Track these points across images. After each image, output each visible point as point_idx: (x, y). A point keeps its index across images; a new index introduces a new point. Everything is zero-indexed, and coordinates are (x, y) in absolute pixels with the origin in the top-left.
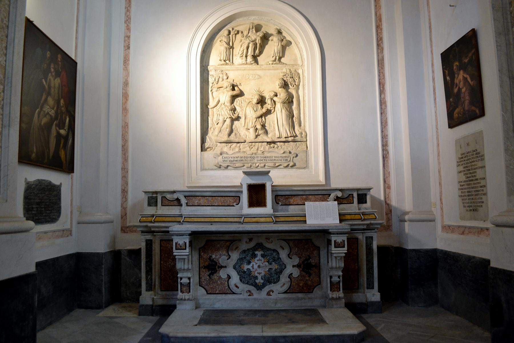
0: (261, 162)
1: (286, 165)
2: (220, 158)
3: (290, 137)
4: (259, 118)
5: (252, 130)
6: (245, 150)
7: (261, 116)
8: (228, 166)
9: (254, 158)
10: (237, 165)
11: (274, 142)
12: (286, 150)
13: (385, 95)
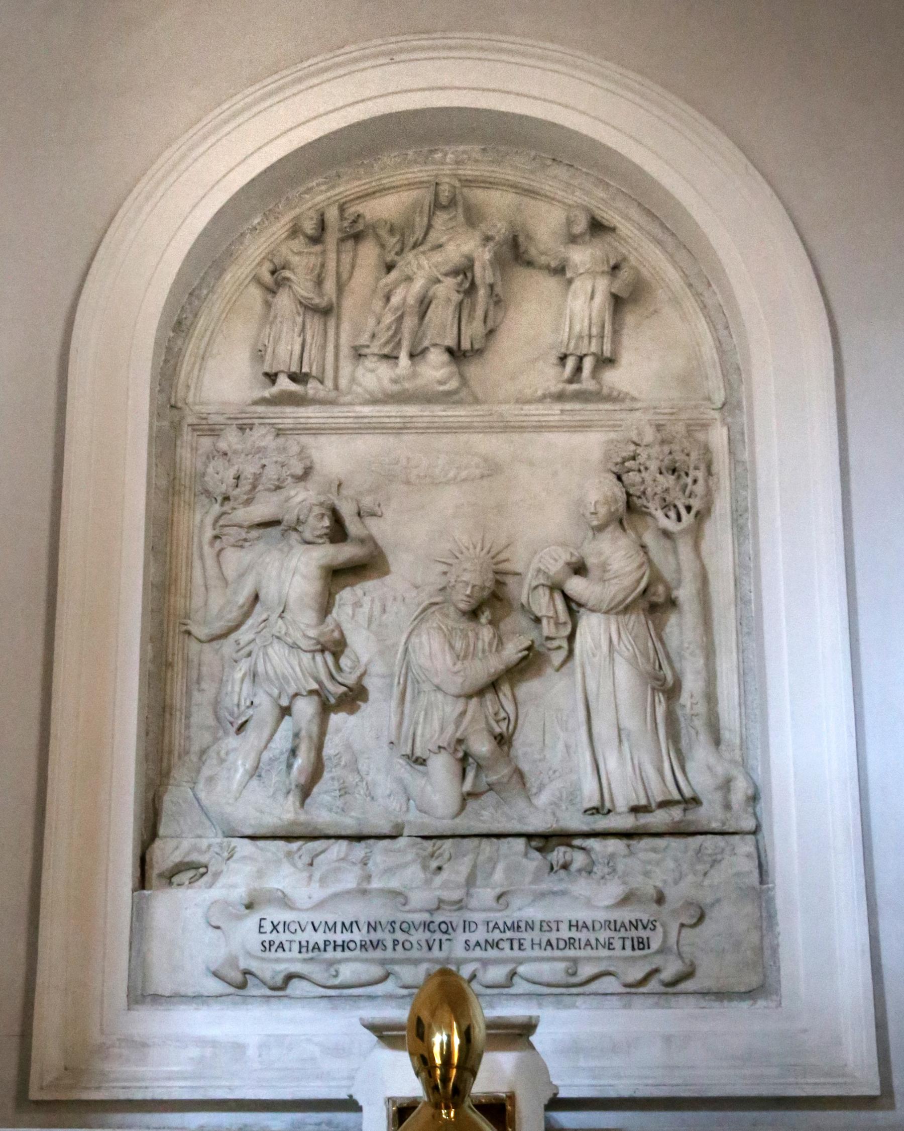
0: (492, 953)
1: (636, 974)
2: (246, 934)
3: (664, 804)
4: (480, 693)
5: (441, 767)
6: (394, 883)
7: (494, 685)
8: (290, 977)
9: (447, 928)
10: (347, 972)
11: (564, 837)
12: (637, 882)
13: (309, 757)
